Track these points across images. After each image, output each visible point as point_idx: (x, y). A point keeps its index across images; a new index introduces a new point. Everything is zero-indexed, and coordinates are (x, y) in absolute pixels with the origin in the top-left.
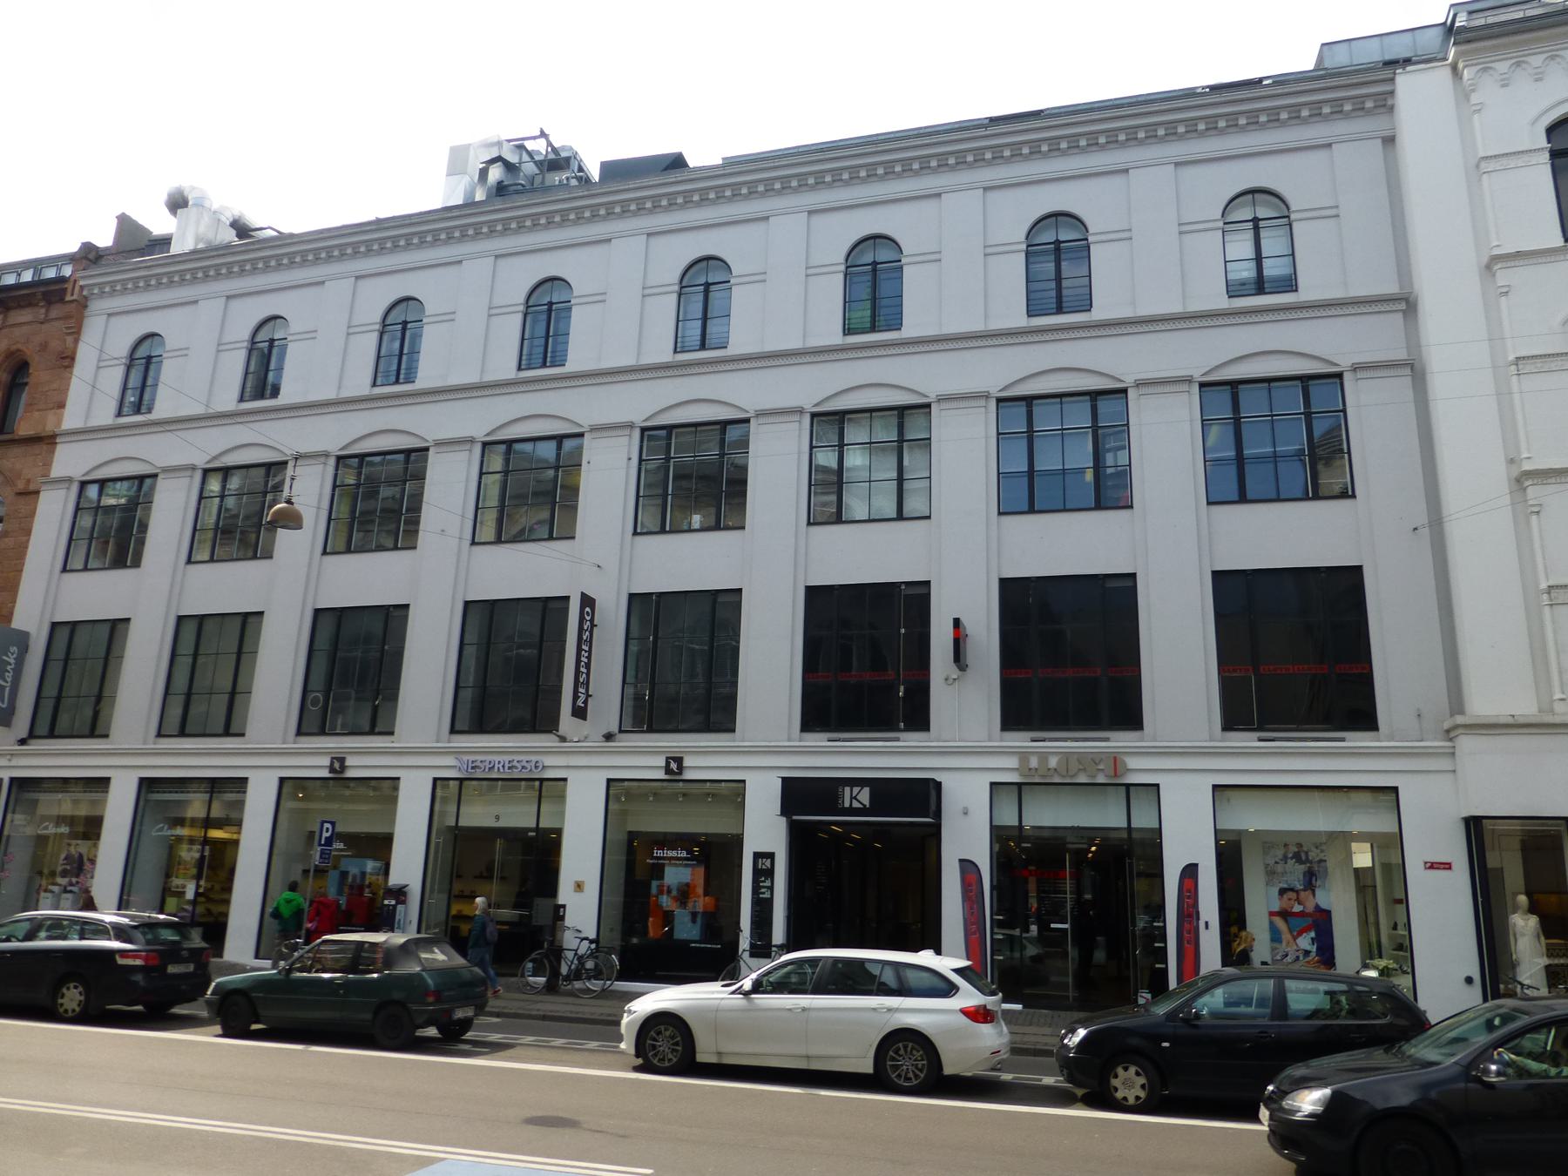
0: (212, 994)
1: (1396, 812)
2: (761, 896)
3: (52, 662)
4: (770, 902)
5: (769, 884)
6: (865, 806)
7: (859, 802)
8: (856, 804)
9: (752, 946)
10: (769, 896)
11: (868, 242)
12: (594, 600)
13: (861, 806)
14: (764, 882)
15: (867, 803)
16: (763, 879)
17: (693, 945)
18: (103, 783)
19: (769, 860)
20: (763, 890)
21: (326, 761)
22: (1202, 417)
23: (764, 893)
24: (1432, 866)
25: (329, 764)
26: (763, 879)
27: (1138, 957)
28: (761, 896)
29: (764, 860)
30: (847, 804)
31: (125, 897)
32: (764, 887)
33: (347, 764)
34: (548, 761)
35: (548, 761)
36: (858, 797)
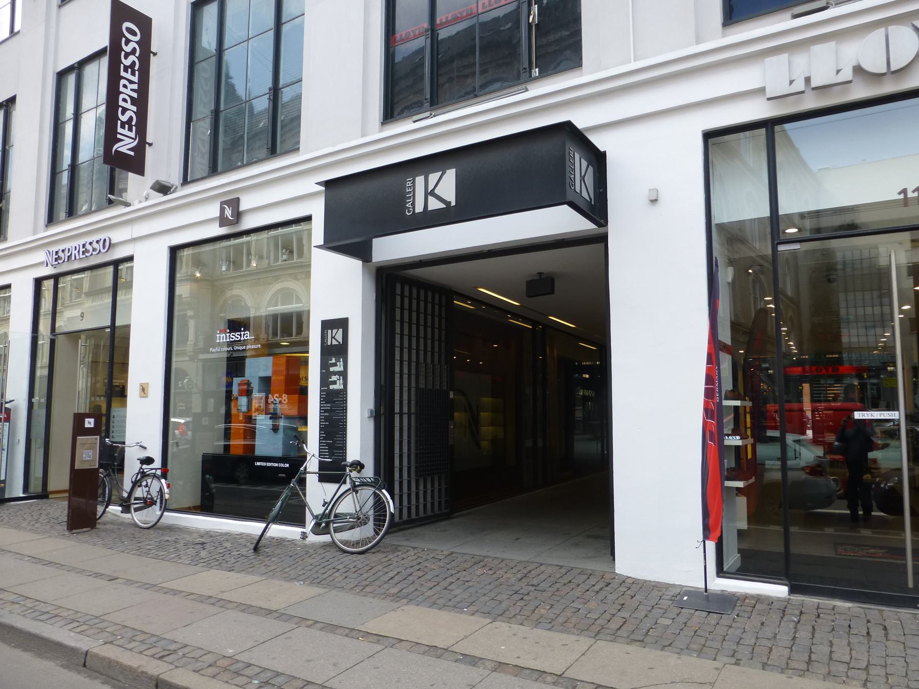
1: (727, 138)
2: (332, 387)
3: (226, 51)
4: (343, 394)
5: (342, 369)
6: (447, 203)
8: (434, 204)
9: (322, 465)
10: (342, 387)
12: (151, 19)
14: (335, 365)
16: (333, 361)
17: (259, 464)
18: (308, 219)
19: (341, 330)
20: (334, 378)
21: (214, 210)
23: (334, 383)
25: (218, 215)
26: (333, 361)
28: (332, 387)
29: (335, 331)
30: (419, 208)
31: (529, 443)
32: (335, 373)
33: (243, 207)
34: (117, 236)
35: (117, 236)
36: (436, 191)
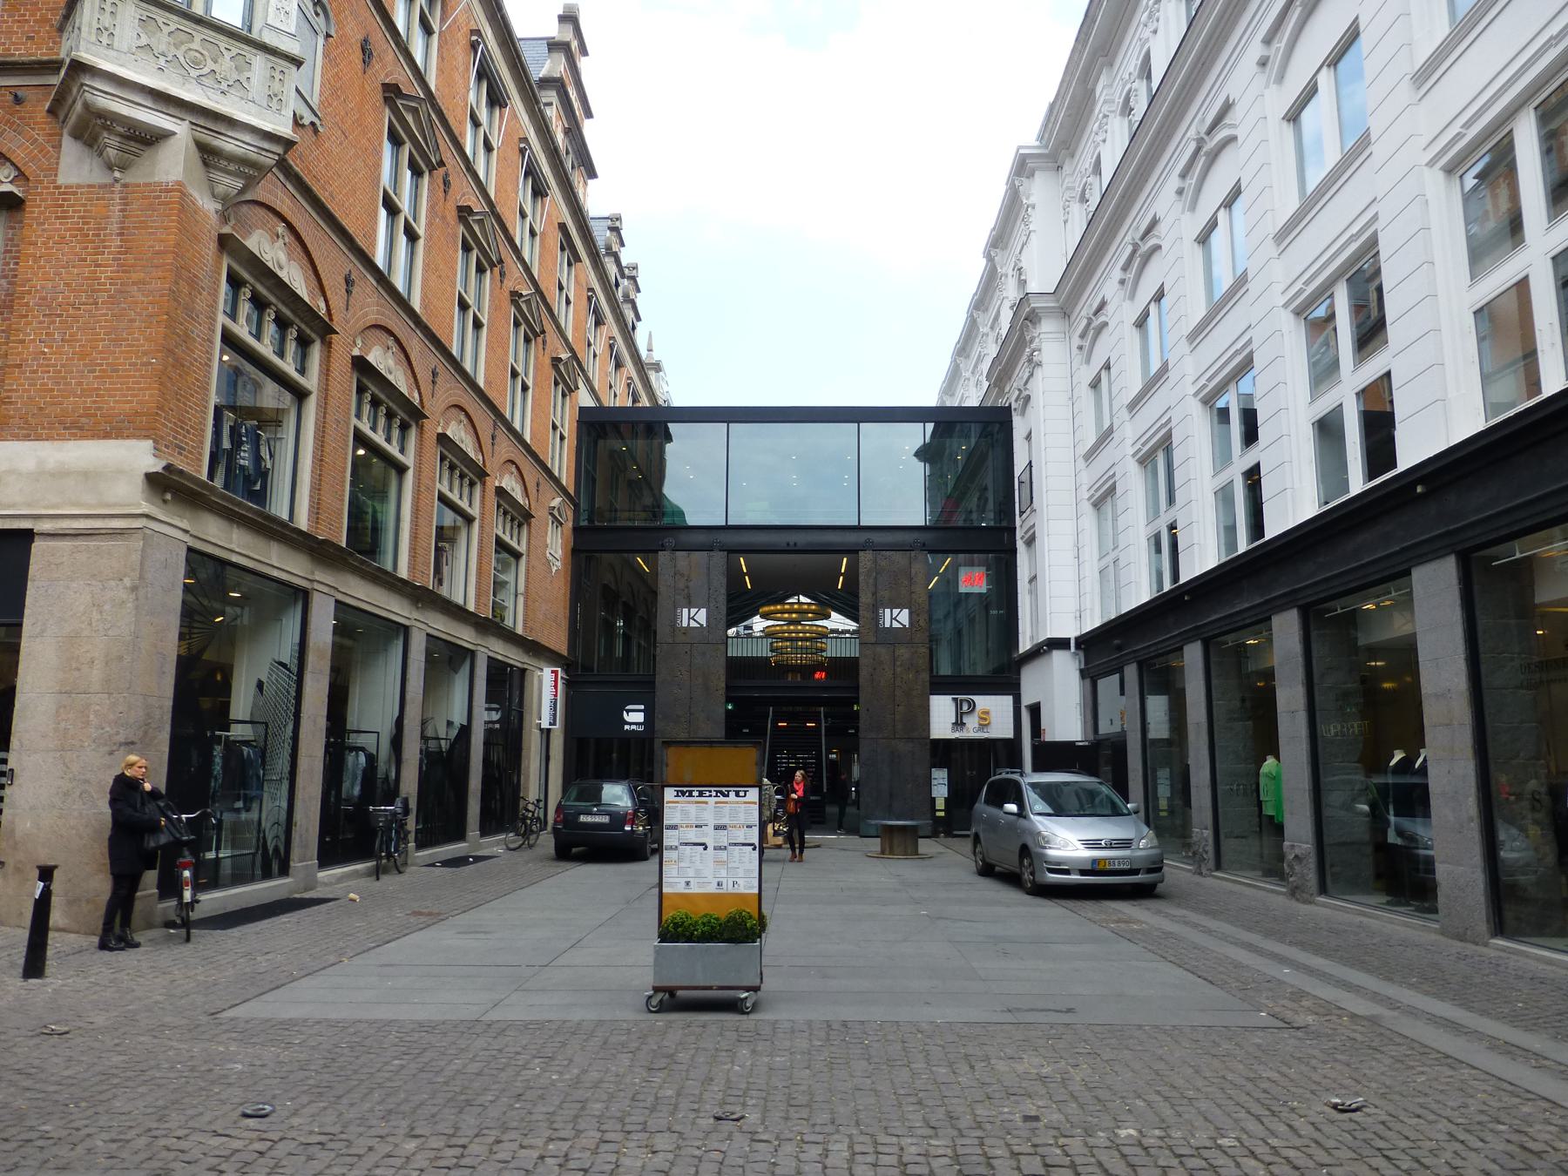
30: (685, 624)
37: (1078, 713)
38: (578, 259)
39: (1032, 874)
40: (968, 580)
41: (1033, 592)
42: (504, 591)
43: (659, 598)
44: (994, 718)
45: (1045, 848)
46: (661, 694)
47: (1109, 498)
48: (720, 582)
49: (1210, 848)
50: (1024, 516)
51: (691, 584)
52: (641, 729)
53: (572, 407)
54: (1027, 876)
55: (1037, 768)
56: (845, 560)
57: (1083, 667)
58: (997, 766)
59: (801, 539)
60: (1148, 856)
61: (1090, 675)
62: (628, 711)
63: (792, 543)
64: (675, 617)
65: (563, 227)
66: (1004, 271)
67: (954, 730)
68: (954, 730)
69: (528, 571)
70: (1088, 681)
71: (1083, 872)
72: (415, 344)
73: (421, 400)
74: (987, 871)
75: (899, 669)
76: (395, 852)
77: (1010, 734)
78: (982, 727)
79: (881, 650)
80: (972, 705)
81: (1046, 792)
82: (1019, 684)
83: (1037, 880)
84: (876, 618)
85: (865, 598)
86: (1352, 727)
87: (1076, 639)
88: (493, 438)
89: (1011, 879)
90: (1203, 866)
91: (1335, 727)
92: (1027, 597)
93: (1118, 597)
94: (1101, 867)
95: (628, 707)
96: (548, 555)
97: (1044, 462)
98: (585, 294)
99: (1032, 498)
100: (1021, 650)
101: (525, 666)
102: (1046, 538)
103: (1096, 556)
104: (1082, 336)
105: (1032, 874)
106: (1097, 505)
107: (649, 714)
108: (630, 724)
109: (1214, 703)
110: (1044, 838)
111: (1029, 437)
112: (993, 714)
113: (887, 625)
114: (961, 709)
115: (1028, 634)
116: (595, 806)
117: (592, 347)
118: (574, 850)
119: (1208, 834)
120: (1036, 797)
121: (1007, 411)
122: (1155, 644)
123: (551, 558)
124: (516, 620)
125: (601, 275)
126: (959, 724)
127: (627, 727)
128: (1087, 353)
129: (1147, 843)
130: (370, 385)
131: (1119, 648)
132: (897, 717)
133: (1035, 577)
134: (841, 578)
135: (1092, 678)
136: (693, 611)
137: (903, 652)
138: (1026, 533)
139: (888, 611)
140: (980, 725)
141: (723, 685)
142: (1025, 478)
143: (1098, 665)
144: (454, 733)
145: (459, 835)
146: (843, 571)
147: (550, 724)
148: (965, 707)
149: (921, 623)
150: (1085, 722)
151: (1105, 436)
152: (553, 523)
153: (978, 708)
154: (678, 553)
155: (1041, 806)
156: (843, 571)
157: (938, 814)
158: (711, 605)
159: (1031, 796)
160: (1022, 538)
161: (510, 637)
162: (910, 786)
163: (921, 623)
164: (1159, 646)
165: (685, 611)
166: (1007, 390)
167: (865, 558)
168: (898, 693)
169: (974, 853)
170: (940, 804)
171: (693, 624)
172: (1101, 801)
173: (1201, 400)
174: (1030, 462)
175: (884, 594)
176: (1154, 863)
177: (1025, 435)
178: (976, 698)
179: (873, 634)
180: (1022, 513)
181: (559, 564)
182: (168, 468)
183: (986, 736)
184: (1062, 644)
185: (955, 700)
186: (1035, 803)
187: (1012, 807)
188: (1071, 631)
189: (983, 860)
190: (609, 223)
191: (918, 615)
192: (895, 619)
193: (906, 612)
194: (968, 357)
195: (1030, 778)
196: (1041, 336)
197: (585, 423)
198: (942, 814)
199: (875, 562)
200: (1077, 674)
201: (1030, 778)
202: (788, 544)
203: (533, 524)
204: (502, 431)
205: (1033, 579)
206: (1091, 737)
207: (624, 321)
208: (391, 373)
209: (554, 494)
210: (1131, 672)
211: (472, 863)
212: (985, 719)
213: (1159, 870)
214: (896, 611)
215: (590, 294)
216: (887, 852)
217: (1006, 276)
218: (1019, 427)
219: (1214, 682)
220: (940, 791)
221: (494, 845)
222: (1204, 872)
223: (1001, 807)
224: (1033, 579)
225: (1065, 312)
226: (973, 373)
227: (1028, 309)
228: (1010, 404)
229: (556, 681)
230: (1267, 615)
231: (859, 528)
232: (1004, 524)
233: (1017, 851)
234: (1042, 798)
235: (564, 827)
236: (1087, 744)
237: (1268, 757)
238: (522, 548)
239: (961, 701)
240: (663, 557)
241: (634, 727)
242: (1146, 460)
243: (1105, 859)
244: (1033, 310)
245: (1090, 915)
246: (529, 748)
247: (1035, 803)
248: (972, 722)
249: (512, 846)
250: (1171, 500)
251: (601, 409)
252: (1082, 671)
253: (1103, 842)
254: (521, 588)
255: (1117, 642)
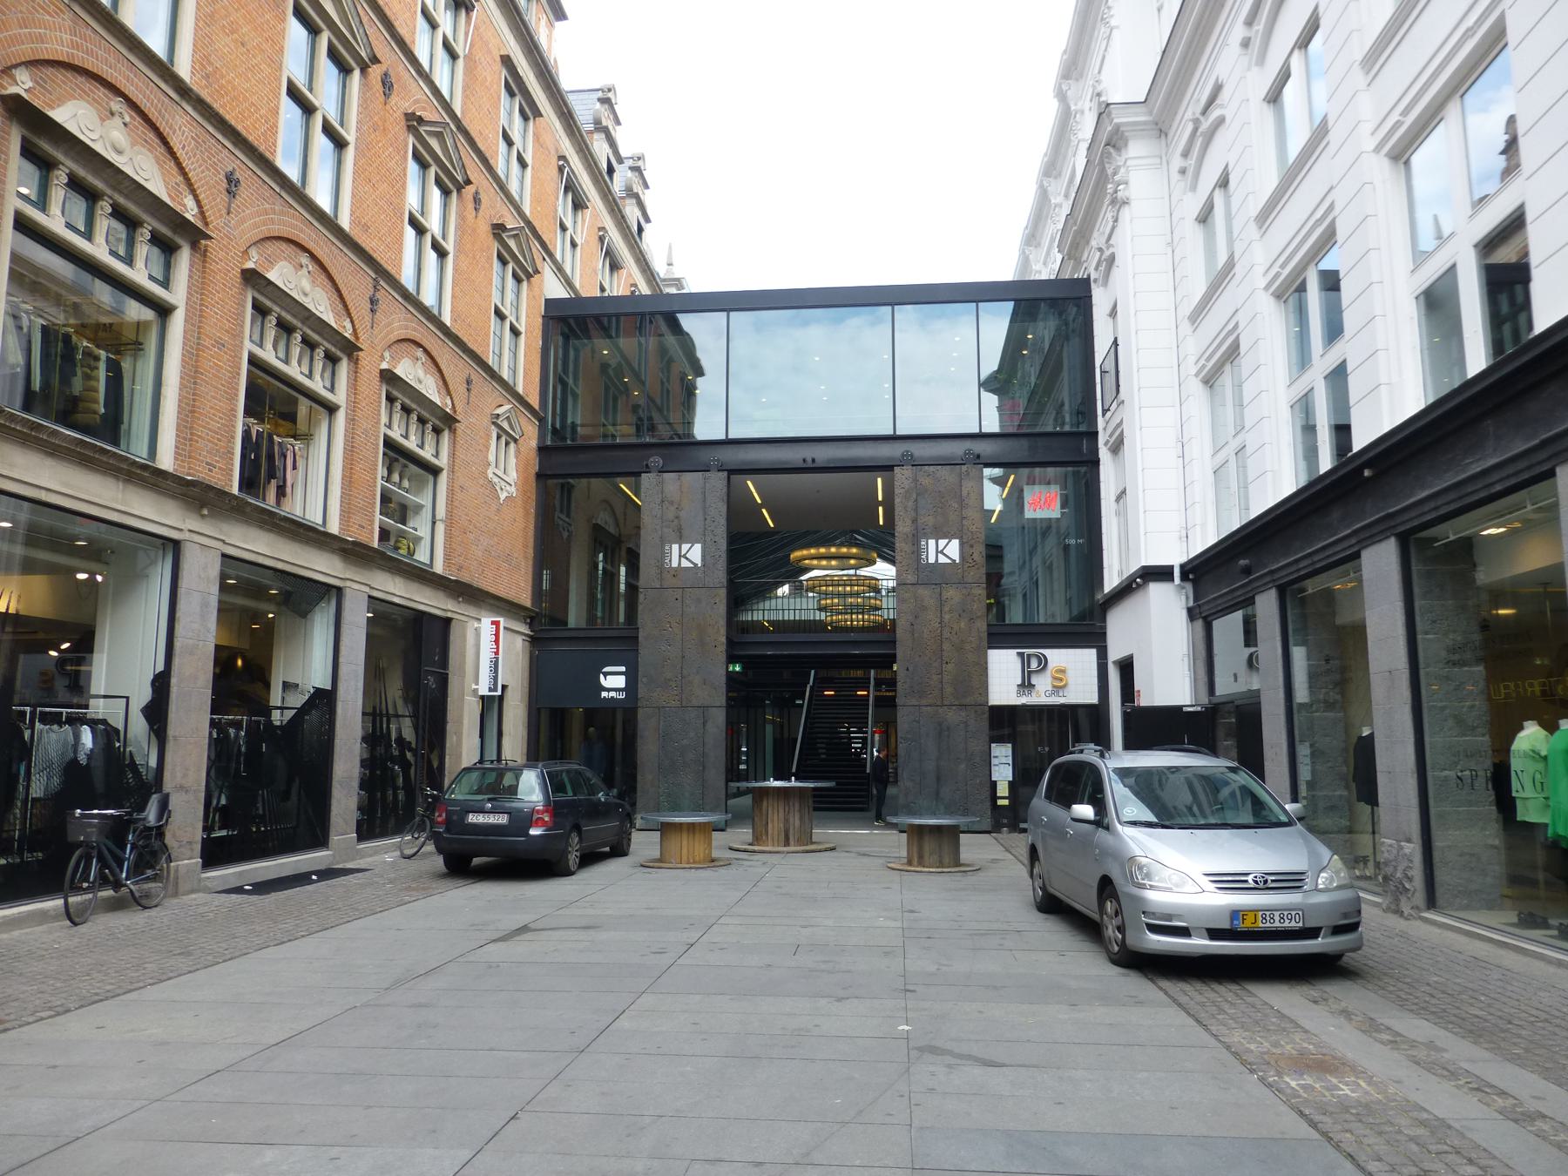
0: (1213, 751)
6: (696, 565)
7: (690, 561)
11: (67, 205)
13: (949, 561)
15: (957, 558)
22: (626, 315)
24: (1236, 680)
27: (744, 742)
30: (675, 564)
37: (1186, 668)
38: (537, 113)
39: (1121, 929)
40: (1034, 504)
41: (1121, 514)
42: (418, 518)
43: (642, 532)
44: (1072, 678)
45: (1143, 887)
46: (646, 653)
47: (1228, 367)
48: (719, 510)
49: (1417, 872)
50: (1109, 414)
51: (682, 514)
52: (622, 696)
53: (531, 298)
54: (1111, 932)
55: (1131, 744)
56: (879, 480)
57: (1191, 604)
58: (1078, 740)
59: (823, 454)
60: (1333, 904)
61: (1202, 615)
62: (606, 674)
63: (809, 460)
64: (663, 555)
65: (507, 61)
66: (1079, 107)
67: (1019, 694)
68: (1019, 694)
69: (451, 492)
70: (1199, 624)
71: (1214, 934)
72: (182, 125)
73: (202, 213)
74: (1051, 905)
75: (947, 617)
76: (127, 879)
77: (1093, 698)
78: (1058, 689)
79: (923, 592)
80: (1043, 662)
81: (1146, 785)
82: (1105, 633)
83: (1129, 941)
84: (917, 552)
85: (903, 527)
86: (1531, 685)
87: (1182, 566)
88: (373, 301)
89: (1089, 928)
90: (1403, 900)
91: (1506, 687)
92: (1114, 520)
93: (1244, 486)
94: (1248, 924)
95: (606, 669)
96: (490, 475)
97: (1134, 350)
98: (554, 162)
99: (1118, 386)
100: (1107, 589)
101: (449, 615)
102: (1138, 432)
103: (1208, 451)
104: (1185, 154)
105: (1121, 929)
106: (1210, 380)
107: (632, 677)
108: (609, 690)
109: (1419, 637)
110: (1140, 868)
111: (1113, 313)
112: (1070, 673)
113: (932, 560)
114: (1029, 667)
115: (1116, 568)
116: (490, 800)
117: (568, 233)
118: (476, 861)
119: (1413, 849)
120: (1127, 792)
121: (1085, 283)
122: (1310, 555)
123: (496, 480)
124: (431, 550)
125: (579, 144)
126: (1026, 685)
127: (604, 694)
128: (1189, 175)
129: (1331, 880)
130: (60, 156)
131: (1247, 571)
132: (946, 678)
133: (1124, 492)
134: (881, 509)
135: (1205, 618)
136: (685, 547)
137: (952, 594)
138: (1111, 436)
139: (932, 542)
140: (1054, 686)
141: (724, 639)
142: (1110, 366)
143: (1215, 599)
144: (297, 700)
145: (317, 837)
146: (880, 498)
147: (490, 690)
148: (1034, 664)
149: (976, 557)
150: (1195, 680)
151: (1221, 279)
152: (499, 437)
153: (1051, 665)
154: (666, 475)
155: (1134, 809)
156: (880, 498)
157: (1000, 802)
158: (708, 539)
159: (1117, 791)
160: (1106, 444)
161: (422, 576)
162: (963, 766)
163: (976, 557)
164: (1316, 558)
165: (675, 547)
166: (1084, 258)
167: (902, 476)
168: (946, 646)
169: (1032, 875)
170: (1003, 790)
171: (685, 564)
172: (1233, 794)
173: (1387, 155)
174: (1116, 339)
175: (928, 520)
176: (1345, 915)
177: (1108, 309)
178: (1047, 652)
179: (919, 576)
180: (1105, 412)
181: (513, 490)
182: (1359, 800)
183: (1062, 701)
184: (1160, 574)
185: (1021, 655)
186: (1126, 804)
187: (1085, 810)
188: (1175, 557)
189: (1043, 888)
190: (600, 94)
191: (972, 546)
192: (942, 552)
193: (955, 543)
194: (1038, 245)
195: (1118, 760)
196: (1129, 163)
197: (552, 318)
198: (1006, 802)
199: (915, 480)
200: (1184, 613)
201: (1118, 760)
202: (804, 460)
203: (459, 432)
204: (387, 295)
205: (1121, 495)
206: (1205, 700)
207: (628, 227)
208: (119, 152)
209: (501, 400)
210: (1267, 605)
211: (315, 882)
212: (1061, 680)
213: (1353, 927)
214: (942, 543)
215: (561, 163)
216: (915, 861)
217: (1082, 112)
218: (1100, 301)
219: (1418, 603)
220: (1003, 773)
221: (385, 853)
222: (1407, 911)
223: (1069, 807)
224: (1121, 495)
225: (1161, 130)
226: (1045, 264)
227: (1109, 128)
228: (1089, 276)
229: (497, 635)
230: (1545, 467)
231: (894, 438)
232: (1083, 428)
233: (1095, 885)
234: (1137, 794)
235: (448, 830)
236: (1199, 709)
237: (1526, 724)
238: (443, 461)
239: (1029, 656)
240: (647, 480)
241: (612, 694)
242: (1291, 292)
243: (1254, 911)
244: (1117, 128)
245: (1237, 1037)
246: (460, 722)
247: (1126, 804)
248: (1043, 683)
249: (409, 852)
250: (1334, 330)
251: (577, 301)
252: (1190, 610)
253: (1250, 878)
254: (441, 512)
255: (1243, 562)
